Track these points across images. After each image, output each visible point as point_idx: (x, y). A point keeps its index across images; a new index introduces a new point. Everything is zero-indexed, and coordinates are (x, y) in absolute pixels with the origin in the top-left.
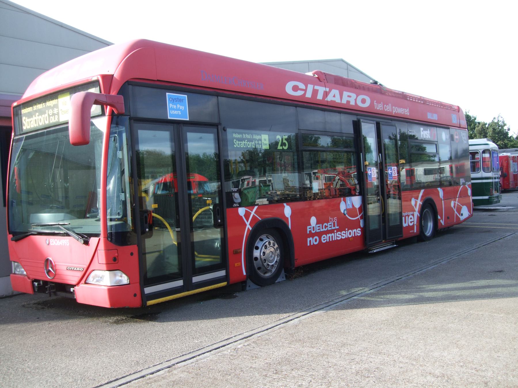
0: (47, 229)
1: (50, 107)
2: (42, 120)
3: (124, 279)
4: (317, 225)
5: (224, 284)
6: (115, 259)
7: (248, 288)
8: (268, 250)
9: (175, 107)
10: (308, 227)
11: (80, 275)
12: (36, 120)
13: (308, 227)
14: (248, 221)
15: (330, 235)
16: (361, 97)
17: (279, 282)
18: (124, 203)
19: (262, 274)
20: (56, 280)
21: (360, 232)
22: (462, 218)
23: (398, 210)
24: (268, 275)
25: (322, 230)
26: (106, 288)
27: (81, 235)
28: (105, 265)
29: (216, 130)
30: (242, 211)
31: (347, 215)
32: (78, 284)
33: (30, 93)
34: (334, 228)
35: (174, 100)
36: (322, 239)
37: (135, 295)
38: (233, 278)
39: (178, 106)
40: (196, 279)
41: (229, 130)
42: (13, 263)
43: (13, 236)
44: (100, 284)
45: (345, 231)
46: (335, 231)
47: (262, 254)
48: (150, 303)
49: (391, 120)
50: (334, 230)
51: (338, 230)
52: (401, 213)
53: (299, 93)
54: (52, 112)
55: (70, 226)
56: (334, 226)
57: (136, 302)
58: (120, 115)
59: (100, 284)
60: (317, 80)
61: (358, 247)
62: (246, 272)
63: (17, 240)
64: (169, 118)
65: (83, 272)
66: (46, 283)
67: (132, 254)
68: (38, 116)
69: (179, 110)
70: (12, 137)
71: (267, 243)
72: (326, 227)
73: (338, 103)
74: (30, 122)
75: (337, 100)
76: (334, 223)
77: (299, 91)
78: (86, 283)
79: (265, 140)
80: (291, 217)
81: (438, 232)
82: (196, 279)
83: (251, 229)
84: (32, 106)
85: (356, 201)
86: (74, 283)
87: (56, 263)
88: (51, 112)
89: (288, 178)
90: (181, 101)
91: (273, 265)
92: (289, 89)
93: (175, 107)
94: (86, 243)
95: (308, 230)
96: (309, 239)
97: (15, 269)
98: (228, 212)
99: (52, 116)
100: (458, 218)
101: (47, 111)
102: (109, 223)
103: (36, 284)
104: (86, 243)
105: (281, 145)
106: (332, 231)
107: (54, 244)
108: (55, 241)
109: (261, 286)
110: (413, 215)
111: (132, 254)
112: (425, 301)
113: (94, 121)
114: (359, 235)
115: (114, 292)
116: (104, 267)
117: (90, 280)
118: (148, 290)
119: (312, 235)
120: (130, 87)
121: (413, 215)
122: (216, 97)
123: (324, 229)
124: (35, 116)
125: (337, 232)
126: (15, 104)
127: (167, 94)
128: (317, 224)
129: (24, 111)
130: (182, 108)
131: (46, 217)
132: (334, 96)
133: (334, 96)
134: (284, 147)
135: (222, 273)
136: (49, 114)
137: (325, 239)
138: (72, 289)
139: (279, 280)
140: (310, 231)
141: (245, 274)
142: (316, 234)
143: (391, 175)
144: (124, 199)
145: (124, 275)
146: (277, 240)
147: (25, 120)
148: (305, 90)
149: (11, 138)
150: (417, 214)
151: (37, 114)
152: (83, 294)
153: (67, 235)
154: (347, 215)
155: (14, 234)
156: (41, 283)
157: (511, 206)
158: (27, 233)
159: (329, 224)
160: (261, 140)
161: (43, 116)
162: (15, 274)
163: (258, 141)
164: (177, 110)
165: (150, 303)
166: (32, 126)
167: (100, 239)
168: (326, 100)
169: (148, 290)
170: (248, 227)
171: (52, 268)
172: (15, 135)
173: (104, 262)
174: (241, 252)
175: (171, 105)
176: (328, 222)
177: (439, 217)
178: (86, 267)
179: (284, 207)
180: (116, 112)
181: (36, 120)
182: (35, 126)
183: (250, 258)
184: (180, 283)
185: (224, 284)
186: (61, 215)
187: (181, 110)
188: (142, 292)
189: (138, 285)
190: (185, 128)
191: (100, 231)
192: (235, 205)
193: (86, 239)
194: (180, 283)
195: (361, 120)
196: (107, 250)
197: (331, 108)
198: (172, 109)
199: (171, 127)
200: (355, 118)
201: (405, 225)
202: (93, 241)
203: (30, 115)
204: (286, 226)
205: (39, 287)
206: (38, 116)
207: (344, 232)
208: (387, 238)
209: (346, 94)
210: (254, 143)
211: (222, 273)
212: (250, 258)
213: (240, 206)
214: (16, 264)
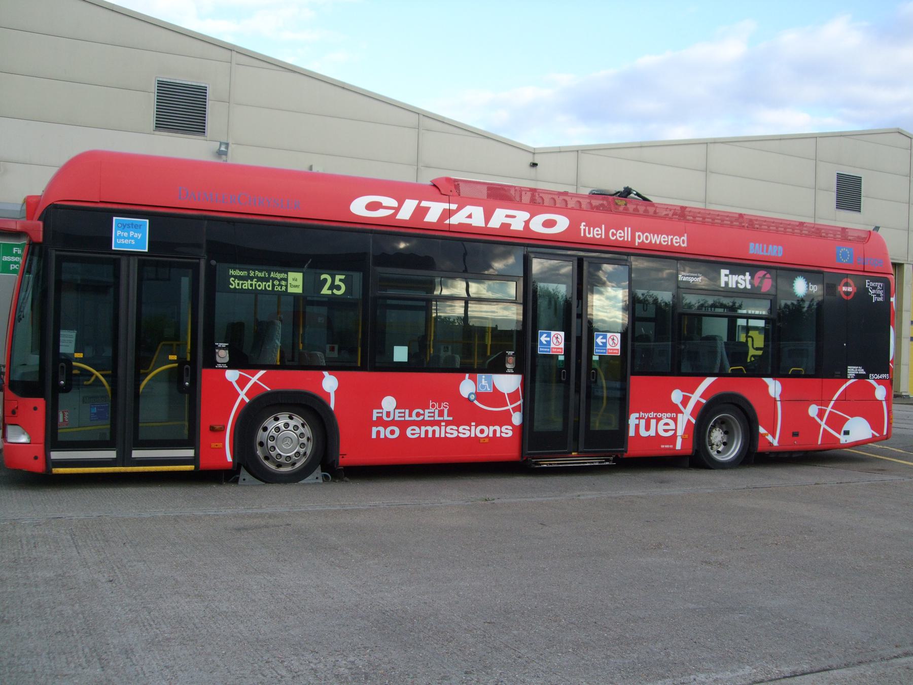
4: (397, 411)
9: (126, 234)
10: (375, 411)
13: (375, 411)
14: (822, 420)
25: (407, 418)
30: (232, 375)
31: (476, 402)
34: (441, 419)
35: (124, 227)
38: (207, 463)
39: (132, 233)
45: (470, 426)
46: (443, 424)
51: (448, 423)
57: (38, 466)
61: (512, 453)
62: (233, 458)
69: (133, 238)
72: (418, 415)
80: (336, 392)
82: (136, 454)
90: (137, 227)
92: (359, 207)
93: (126, 234)
96: (374, 430)
98: (206, 375)
105: (330, 288)
109: (266, 482)
111: (35, 409)
113: (464, 284)
118: (55, 455)
119: (380, 422)
121: (675, 420)
123: (414, 418)
125: (446, 426)
128: (397, 408)
134: (335, 291)
135: (190, 453)
142: (394, 423)
154: (476, 402)
159: (427, 411)
160: (286, 280)
163: (280, 280)
164: (129, 238)
168: (447, 222)
170: (243, 395)
174: (224, 430)
175: (119, 232)
179: (323, 377)
184: (112, 454)
185: (191, 468)
187: (136, 239)
188: (47, 456)
189: (42, 446)
194: (112, 454)
198: (120, 237)
204: (326, 406)
207: (468, 428)
208: (581, 449)
210: (270, 284)
211: (190, 453)
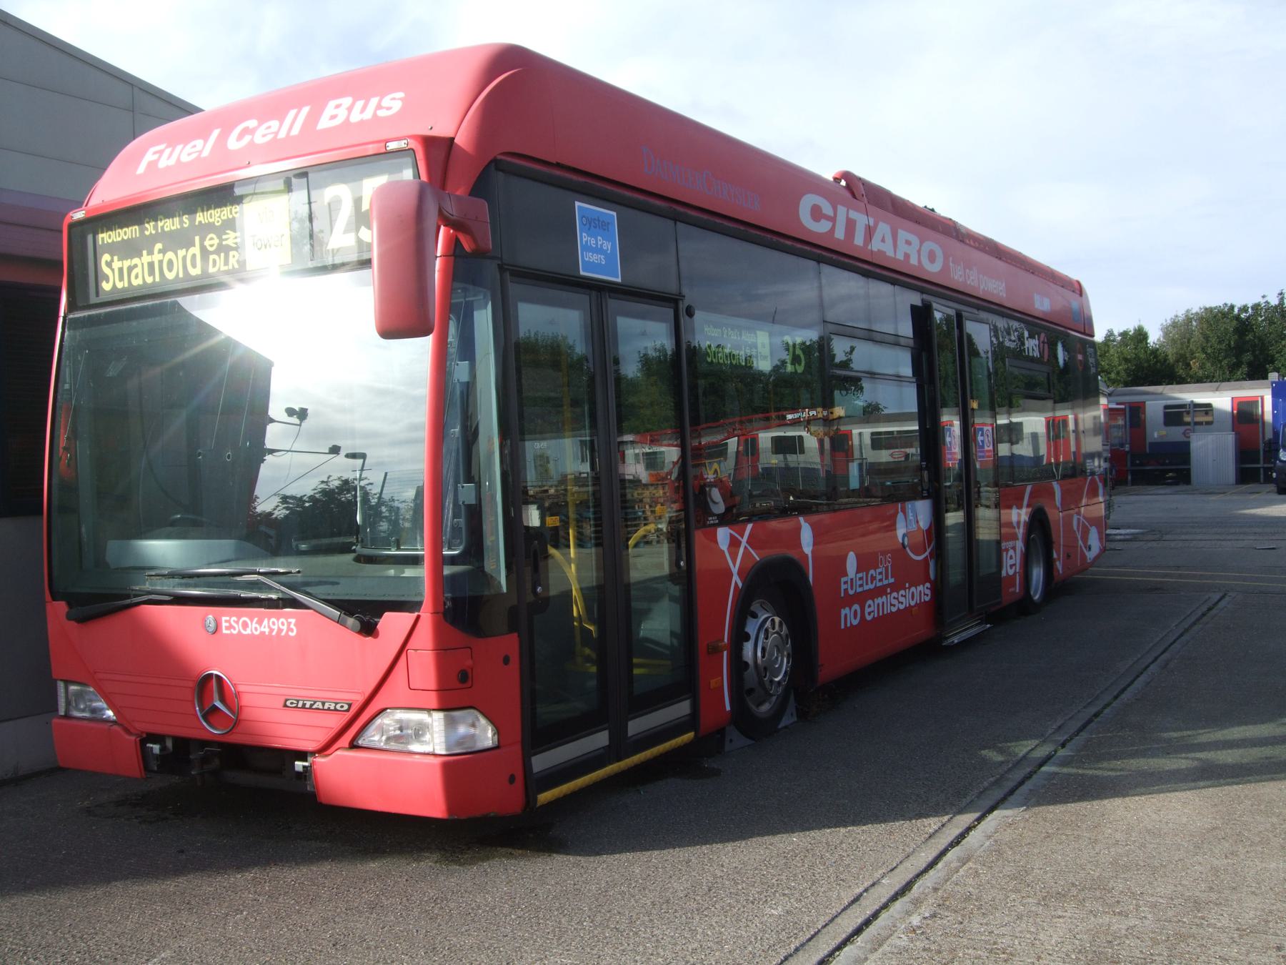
0: (196, 586)
1: (210, 228)
2: (178, 265)
3: (486, 735)
4: (860, 575)
5: (689, 736)
6: (464, 677)
7: (728, 747)
8: (765, 641)
11: (336, 722)
12: (151, 265)
13: (843, 580)
15: (879, 600)
16: (929, 245)
17: (786, 727)
18: (474, 514)
19: (753, 707)
20: (236, 738)
21: (928, 592)
22: (1091, 555)
23: (994, 537)
24: (765, 708)
25: (866, 588)
26: (438, 761)
27: (347, 607)
28: (433, 696)
29: (671, 312)
32: (324, 749)
33: (109, 190)
36: (867, 610)
37: (512, 779)
40: (636, 727)
41: (698, 315)
42: (61, 685)
43: (70, 605)
44: (417, 745)
45: (905, 589)
47: (759, 654)
48: (545, 797)
49: (979, 308)
50: (885, 587)
52: (998, 543)
53: (822, 227)
54: (216, 241)
55: (299, 578)
56: (887, 578)
57: (508, 800)
58: (480, 254)
59: (417, 745)
60: (848, 195)
63: (83, 620)
64: (582, 273)
65: (348, 716)
66: (183, 744)
67: (506, 660)
68: (163, 251)
70: (62, 314)
71: (768, 624)
72: (873, 578)
73: (890, 257)
74: (130, 269)
75: (888, 249)
76: (887, 569)
77: (823, 221)
78: (353, 746)
79: (763, 346)
81: (1054, 589)
82: (636, 727)
83: (740, 585)
84: (140, 222)
85: (921, 511)
86: (310, 746)
87: (241, 688)
88: (212, 241)
89: (549, 453)
91: (779, 682)
94: (368, 629)
95: (843, 587)
96: (843, 612)
97: (68, 703)
98: (699, 537)
99: (217, 252)
100: (1083, 557)
101: (197, 239)
102: (447, 570)
103: (156, 748)
104: (368, 629)
106: (880, 592)
107: (238, 629)
108: (236, 623)
110: (1014, 548)
111: (506, 660)
112: (1220, 776)
114: (927, 599)
115: (459, 768)
116: (433, 700)
117: (373, 737)
118: (542, 762)
119: (849, 600)
120: (501, 175)
122: (671, 223)
124: (151, 253)
126: (79, 215)
127: (577, 204)
129: (105, 237)
130: (607, 246)
131: (163, 550)
132: (883, 240)
133: (883, 240)
135: (682, 709)
136: (203, 248)
137: (873, 609)
138: (299, 765)
139: (787, 720)
140: (846, 590)
141: (728, 708)
143: (983, 447)
144: (472, 500)
145: (483, 721)
146: (786, 619)
147: (109, 264)
148: (833, 220)
149: (58, 316)
150: (1020, 545)
151: (159, 246)
152: (344, 776)
153: (295, 604)
155: (74, 601)
156: (169, 744)
157: (1129, 527)
158: (128, 597)
161: (181, 253)
162: (67, 716)
165: (545, 797)
166: (136, 282)
167: (418, 617)
169: (542, 762)
171: (223, 700)
172: (72, 307)
173: (431, 683)
176: (876, 568)
177: (1055, 556)
178: (359, 699)
180: (467, 246)
181: (151, 265)
182: (149, 280)
183: (738, 665)
184: (601, 739)
185: (689, 736)
186: (226, 546)
188: (527, 766)
189: (518, 748)
190: (613, 304)
191: (421, 594)
192: (712, 520)
193: (365, 613)
194: (601, 739)
195: (935, 305)
196: (443, 649)
197: (878, 271)
198: (588, 248)
199: (583, 298)
200: (916, 299)
201: (635, 575)
202: (393, 624)
203: (129, 250)
205: (164, 757)
206: (163, 251)
209: (903, 235)
211: (682, 709)
212: (738, 665)
213: (721, 524)
214: (73, 688)
